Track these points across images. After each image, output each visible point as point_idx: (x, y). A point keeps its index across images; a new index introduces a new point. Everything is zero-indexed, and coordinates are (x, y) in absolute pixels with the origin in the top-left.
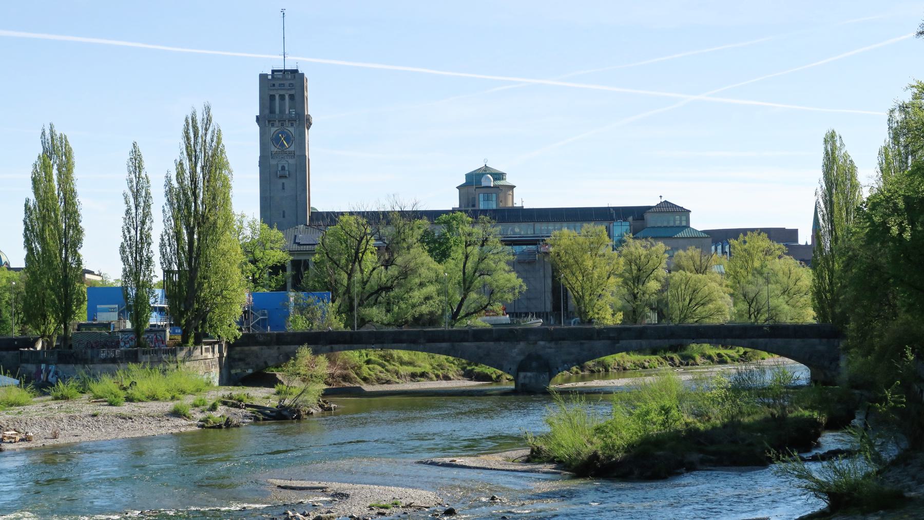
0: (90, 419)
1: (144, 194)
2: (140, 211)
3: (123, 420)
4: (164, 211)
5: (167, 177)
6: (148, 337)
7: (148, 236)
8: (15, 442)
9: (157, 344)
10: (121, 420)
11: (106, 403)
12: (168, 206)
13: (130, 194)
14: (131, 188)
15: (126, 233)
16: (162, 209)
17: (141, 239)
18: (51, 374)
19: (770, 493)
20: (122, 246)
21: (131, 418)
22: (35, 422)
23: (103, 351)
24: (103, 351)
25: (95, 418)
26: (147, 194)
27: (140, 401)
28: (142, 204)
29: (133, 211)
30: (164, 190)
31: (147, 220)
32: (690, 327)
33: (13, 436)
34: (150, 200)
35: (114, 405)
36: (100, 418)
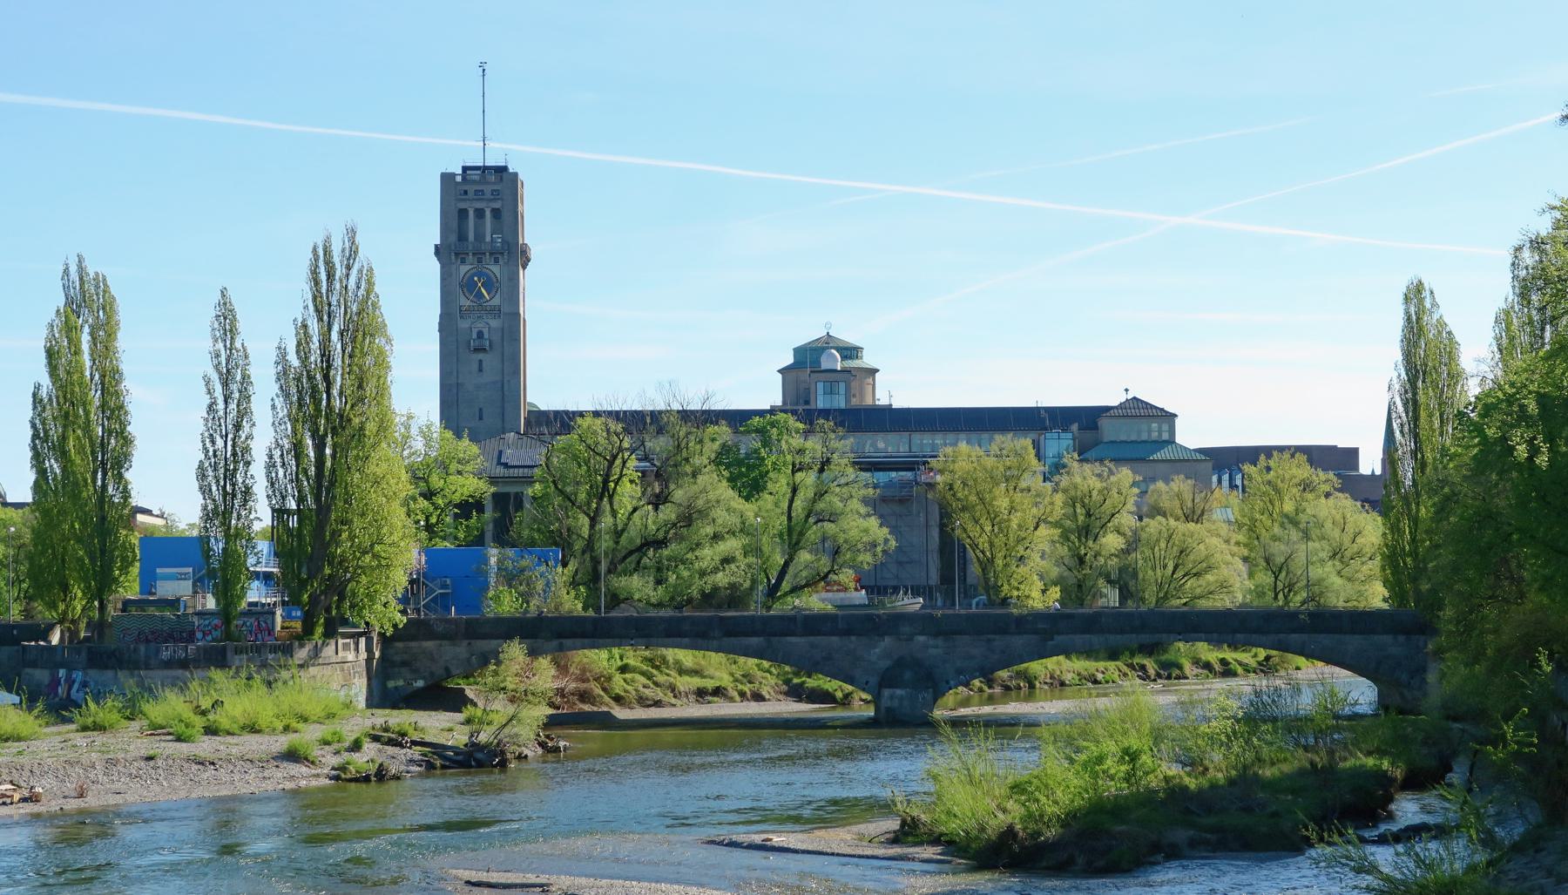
1: (239, 378)
2: (233, 406)
3: (200, 767)
4: (274, 407)
6: (244, 623)
7: (247, 450)
8: (12, 803)
10: (197, 767)
11: (170, 737)
12: (281, 399)
13: (215, 377)
14: (217, 367)
15: (208, 445)
16: (270, 403)
17: (234, 454)
20: (201, 467)
21: (213, 764)
23: (167, 647)
24: (167, 647)
25: (152, 763)
29: (221, 406)
33: (8, 793)
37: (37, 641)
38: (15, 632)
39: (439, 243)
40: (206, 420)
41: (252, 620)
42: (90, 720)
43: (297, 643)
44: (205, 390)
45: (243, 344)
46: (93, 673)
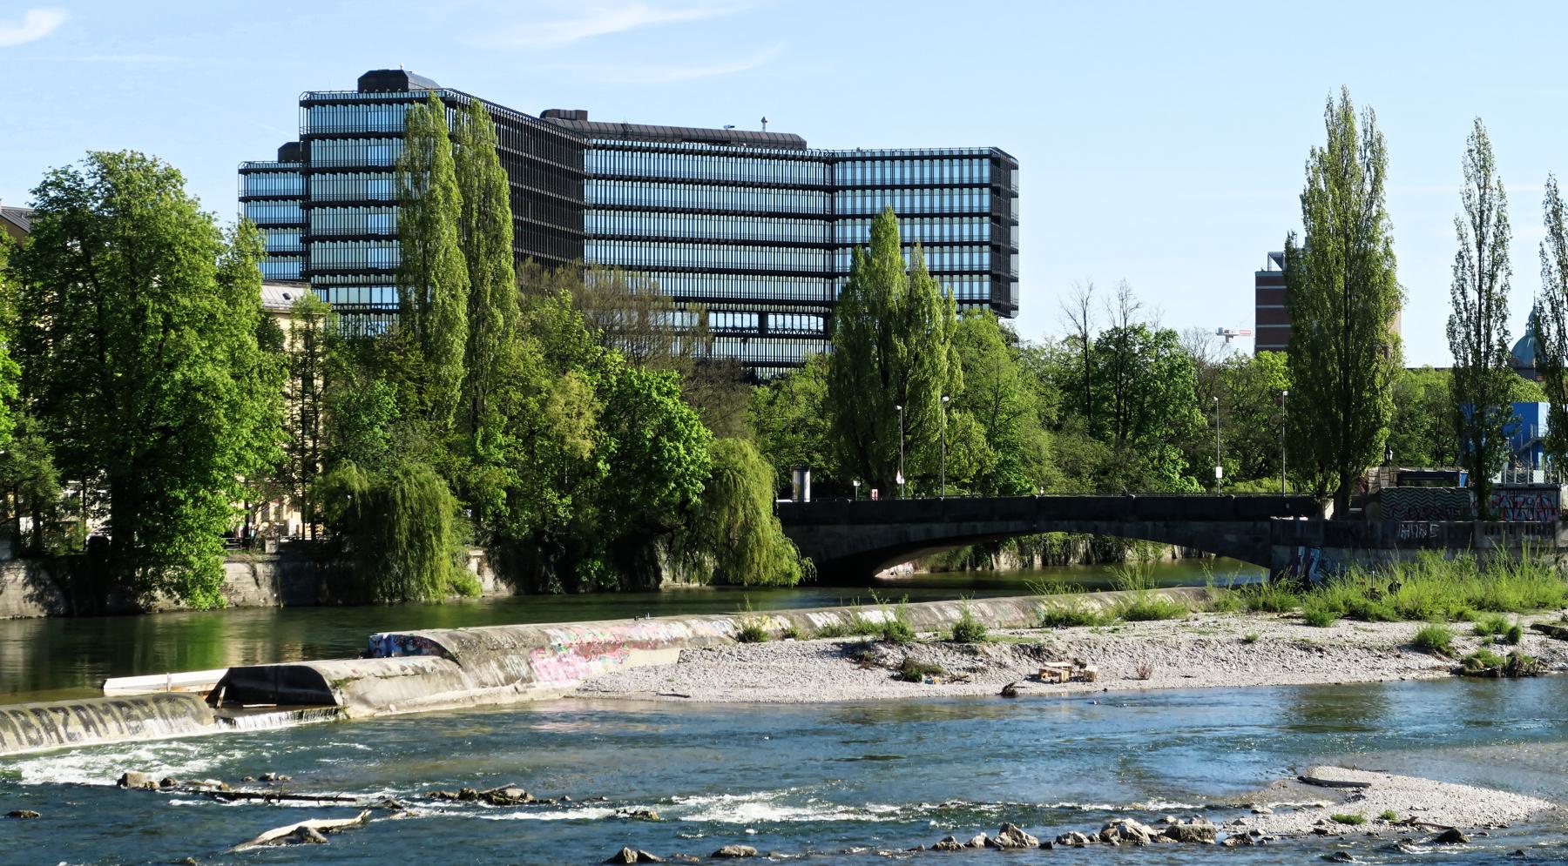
0: (1236, 647)
1: (1494, 220)
2: (1486, 252)
3: (1304, 653)
4: (1542, 253)
5: (1548, 185)
6: (1525, 500)
7: (1501, 302)
8: (1060, 681)
9: (1542, 515)
10: (1299, 652)
11: (1300, 621)
12: (1552, 244)
13: (1468, 219)
14: (1468, 208)
15: (1460, 298)
16: (1539, 249)
17: (1488, 307)
18: (1314, 565)
19: (1034, 667)
20: (1451, 323)
21: (1321, 650)
22: (1122, 649)
23: (1406, 525)
24: (1406, 525)
25: (1248, 647)
26: (1501, 220)
27: (1380, 618)
28: (1490, 240)
29: (1475, 253)
30: (1543, 212)
31: (1499, 272)
32: (1216, 498)
33: (1058, 671)
34: (1507, 232)
35: (1315, 625)
36: (1258, 646)
37: (1297, 516)
38: (1288, 506)
39: (590, 119)
40: (1456, 269)
41: (1534, 497)
42: (1261, 600)
43: (1560, 523)
44: (1456, 234)
45: (1499, 182)
46: (1330, 551)
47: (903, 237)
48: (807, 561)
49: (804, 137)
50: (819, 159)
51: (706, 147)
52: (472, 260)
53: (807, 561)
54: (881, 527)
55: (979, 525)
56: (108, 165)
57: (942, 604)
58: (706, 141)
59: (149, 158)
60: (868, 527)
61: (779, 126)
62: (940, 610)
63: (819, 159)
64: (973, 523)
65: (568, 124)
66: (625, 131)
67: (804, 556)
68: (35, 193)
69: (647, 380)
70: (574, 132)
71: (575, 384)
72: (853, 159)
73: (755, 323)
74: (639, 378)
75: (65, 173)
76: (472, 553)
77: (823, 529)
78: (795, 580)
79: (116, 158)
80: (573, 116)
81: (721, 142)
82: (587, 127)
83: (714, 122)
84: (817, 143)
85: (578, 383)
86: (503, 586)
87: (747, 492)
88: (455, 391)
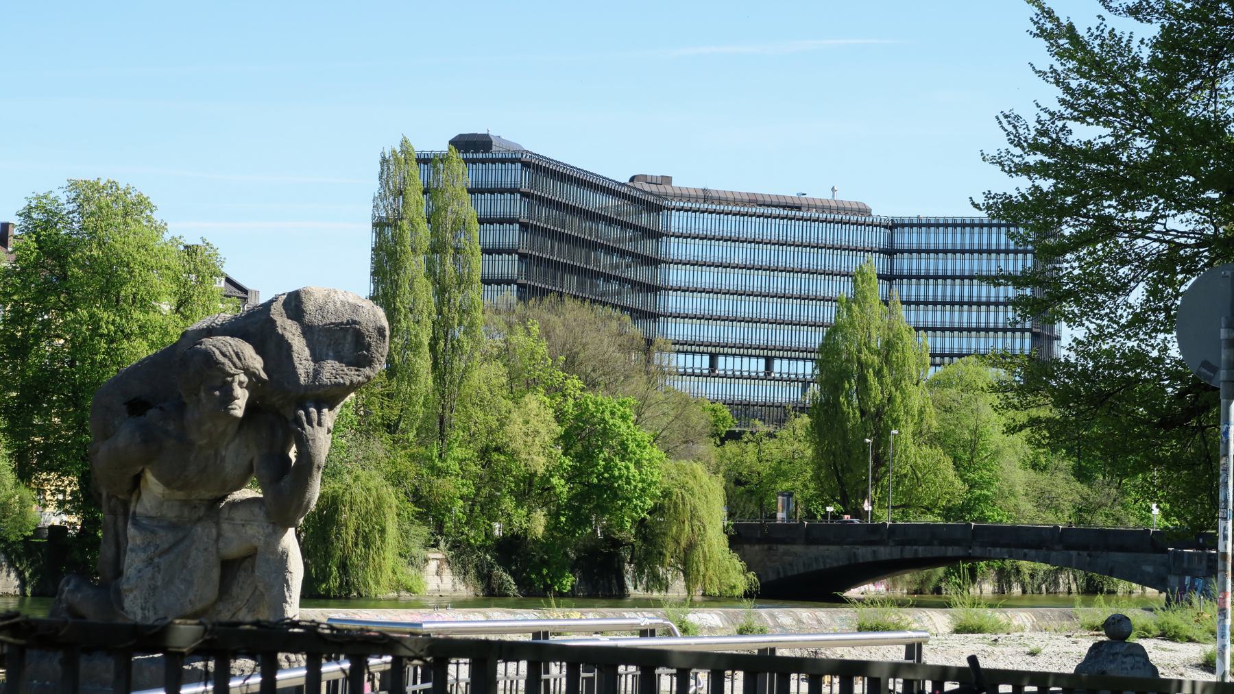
47: (901, 296)
48: (751, 575)
49: (869, 205)
50: (879, 225)
51: (783, 212)
52: (441, 291)
53: (751, 575)
54: (833, 548)
55: (921, 548)
56: (85, 193)
57: (776, 611)
58: (784, 207)
59: (122, 186)
60: (822, 548)
61: (848, 195)
62: (772, 616)
63: (879, 225)
64: (915, 547)
65: (654, 188)
66: (707, 197)
67: (749, 570)
68: (20, 215)
69: (602, 404)
70: (659, 196)
71: (533, 405)
72: (911, 225)
73: (762, 367)
74: (595, 403)
75: (45, 197)
76: (431, 555)
77: (782, 548)
78: (740, 591)
79: (94, 187)
80: (659, 182)
81: (791, 208)
82: (670, 191)
83: (786, 189)
84: (883, 209)
85: (535, 402)
86: (462, 588)
87: (694, 510)
88: (417, 408)
